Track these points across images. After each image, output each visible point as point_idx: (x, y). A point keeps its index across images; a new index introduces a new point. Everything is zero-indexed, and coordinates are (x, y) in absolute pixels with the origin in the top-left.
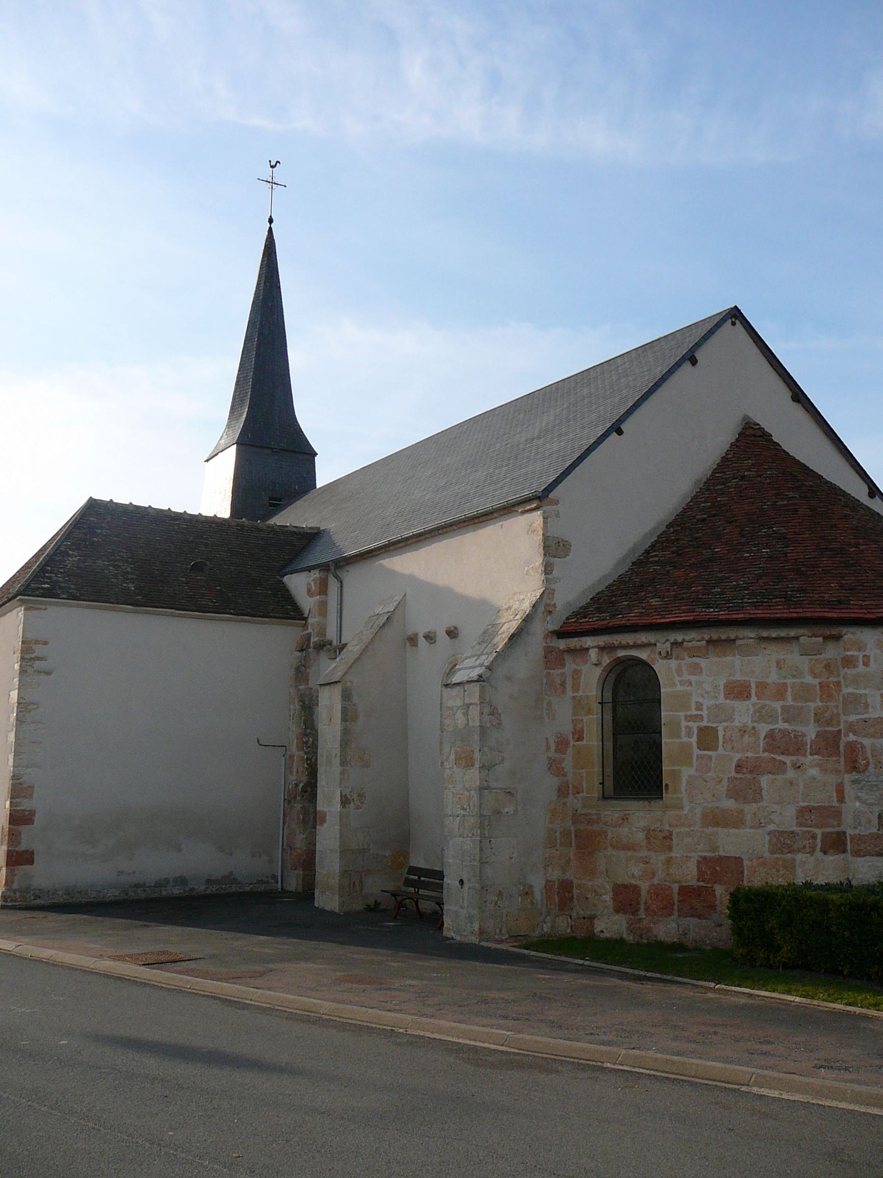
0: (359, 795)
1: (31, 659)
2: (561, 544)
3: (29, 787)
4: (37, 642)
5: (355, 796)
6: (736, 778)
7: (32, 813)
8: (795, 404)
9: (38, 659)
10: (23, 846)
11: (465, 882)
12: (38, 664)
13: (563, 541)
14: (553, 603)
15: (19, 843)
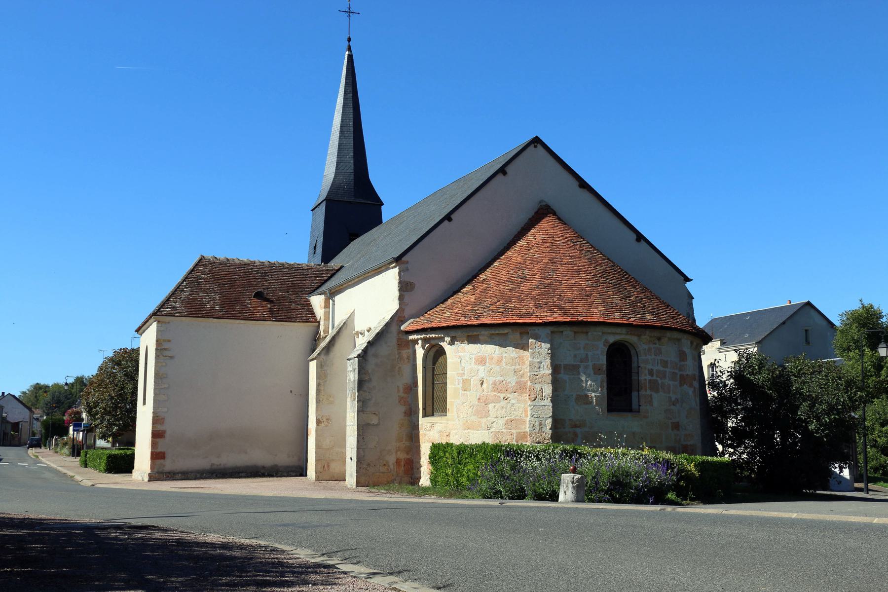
0: (328, 419)
1: (161, 349)
2: (409, 284)
3: (162, 418)
4: (164, 341)
5: (324, 420)
6: (478, 405)
7: (164, 432)
8: (581, 190)
9: (165, 349)
10: (159, 450)
11: (352, 458)
12: (166, 353)
13: (410, 283)
14: (403, 316)
15: (157, 448)
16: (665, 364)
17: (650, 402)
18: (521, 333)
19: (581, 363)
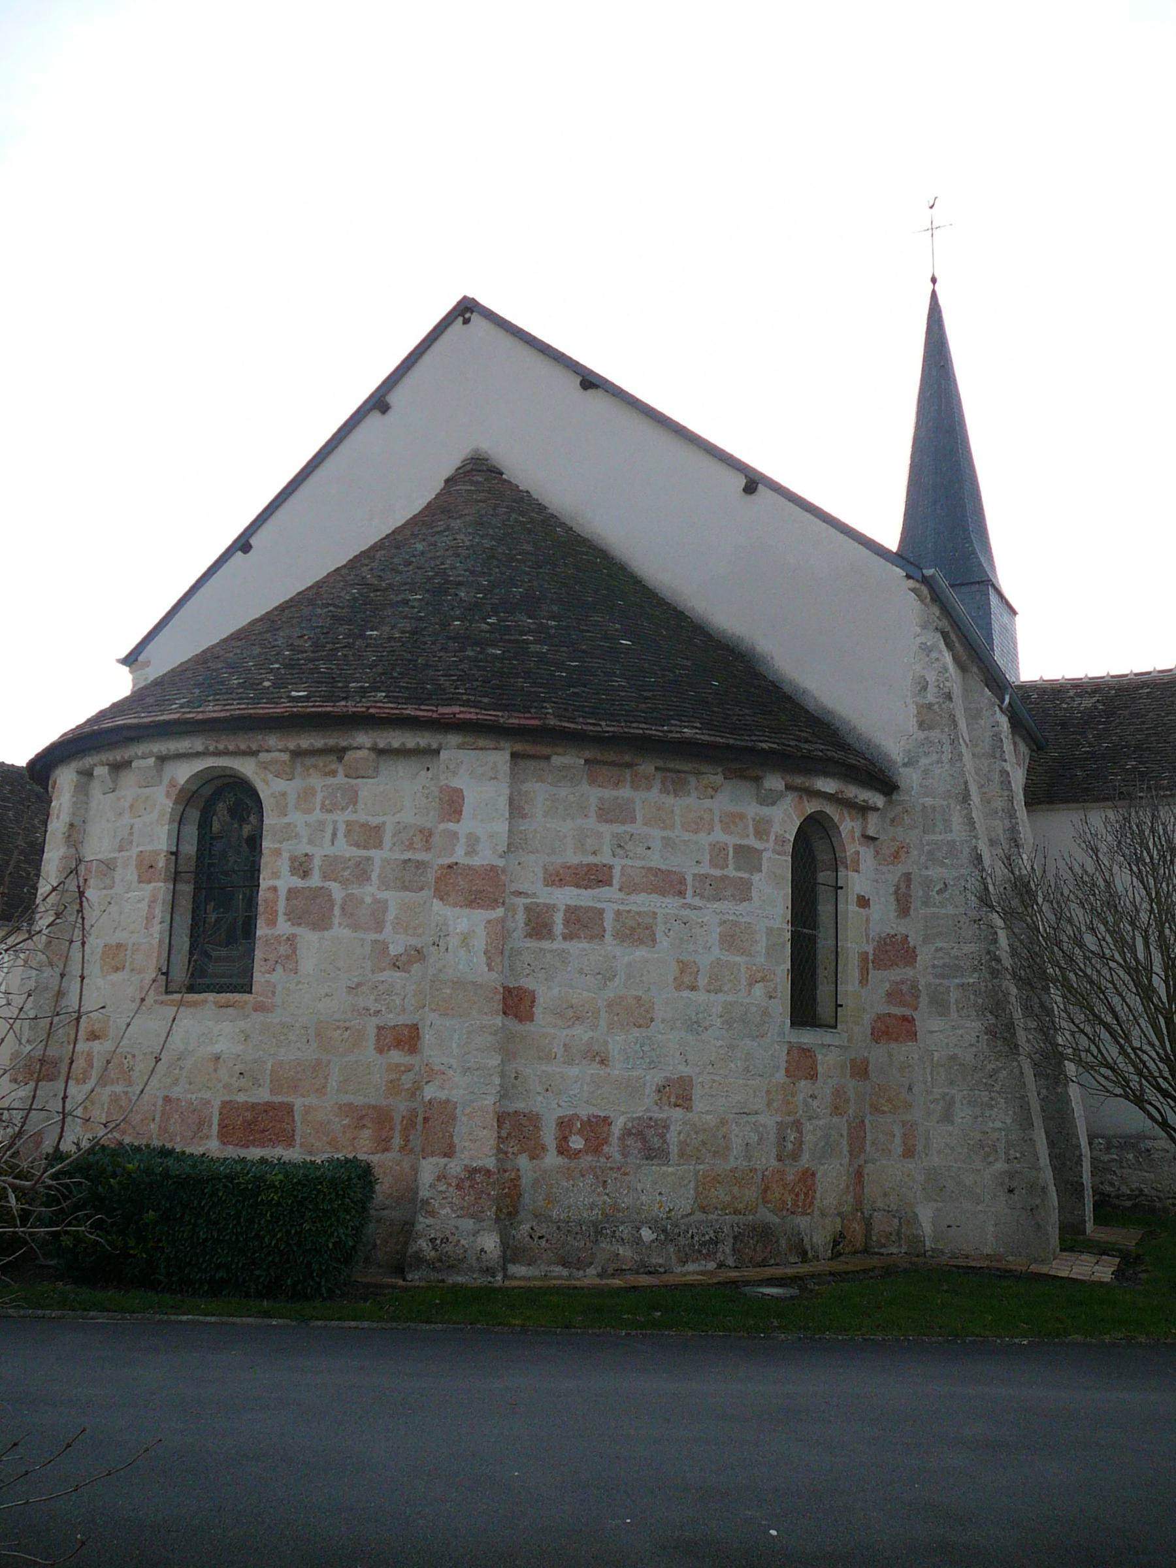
16: (370, 836)
17: (289, 958)
18: (514, 756)
19: (120, 851)
